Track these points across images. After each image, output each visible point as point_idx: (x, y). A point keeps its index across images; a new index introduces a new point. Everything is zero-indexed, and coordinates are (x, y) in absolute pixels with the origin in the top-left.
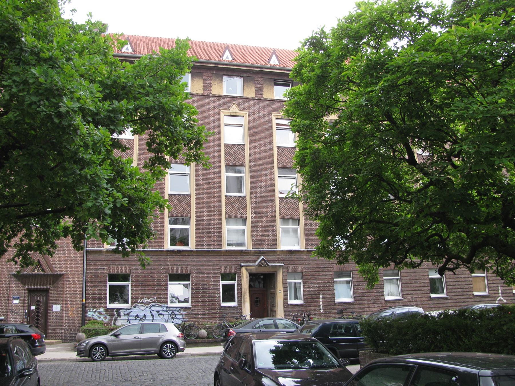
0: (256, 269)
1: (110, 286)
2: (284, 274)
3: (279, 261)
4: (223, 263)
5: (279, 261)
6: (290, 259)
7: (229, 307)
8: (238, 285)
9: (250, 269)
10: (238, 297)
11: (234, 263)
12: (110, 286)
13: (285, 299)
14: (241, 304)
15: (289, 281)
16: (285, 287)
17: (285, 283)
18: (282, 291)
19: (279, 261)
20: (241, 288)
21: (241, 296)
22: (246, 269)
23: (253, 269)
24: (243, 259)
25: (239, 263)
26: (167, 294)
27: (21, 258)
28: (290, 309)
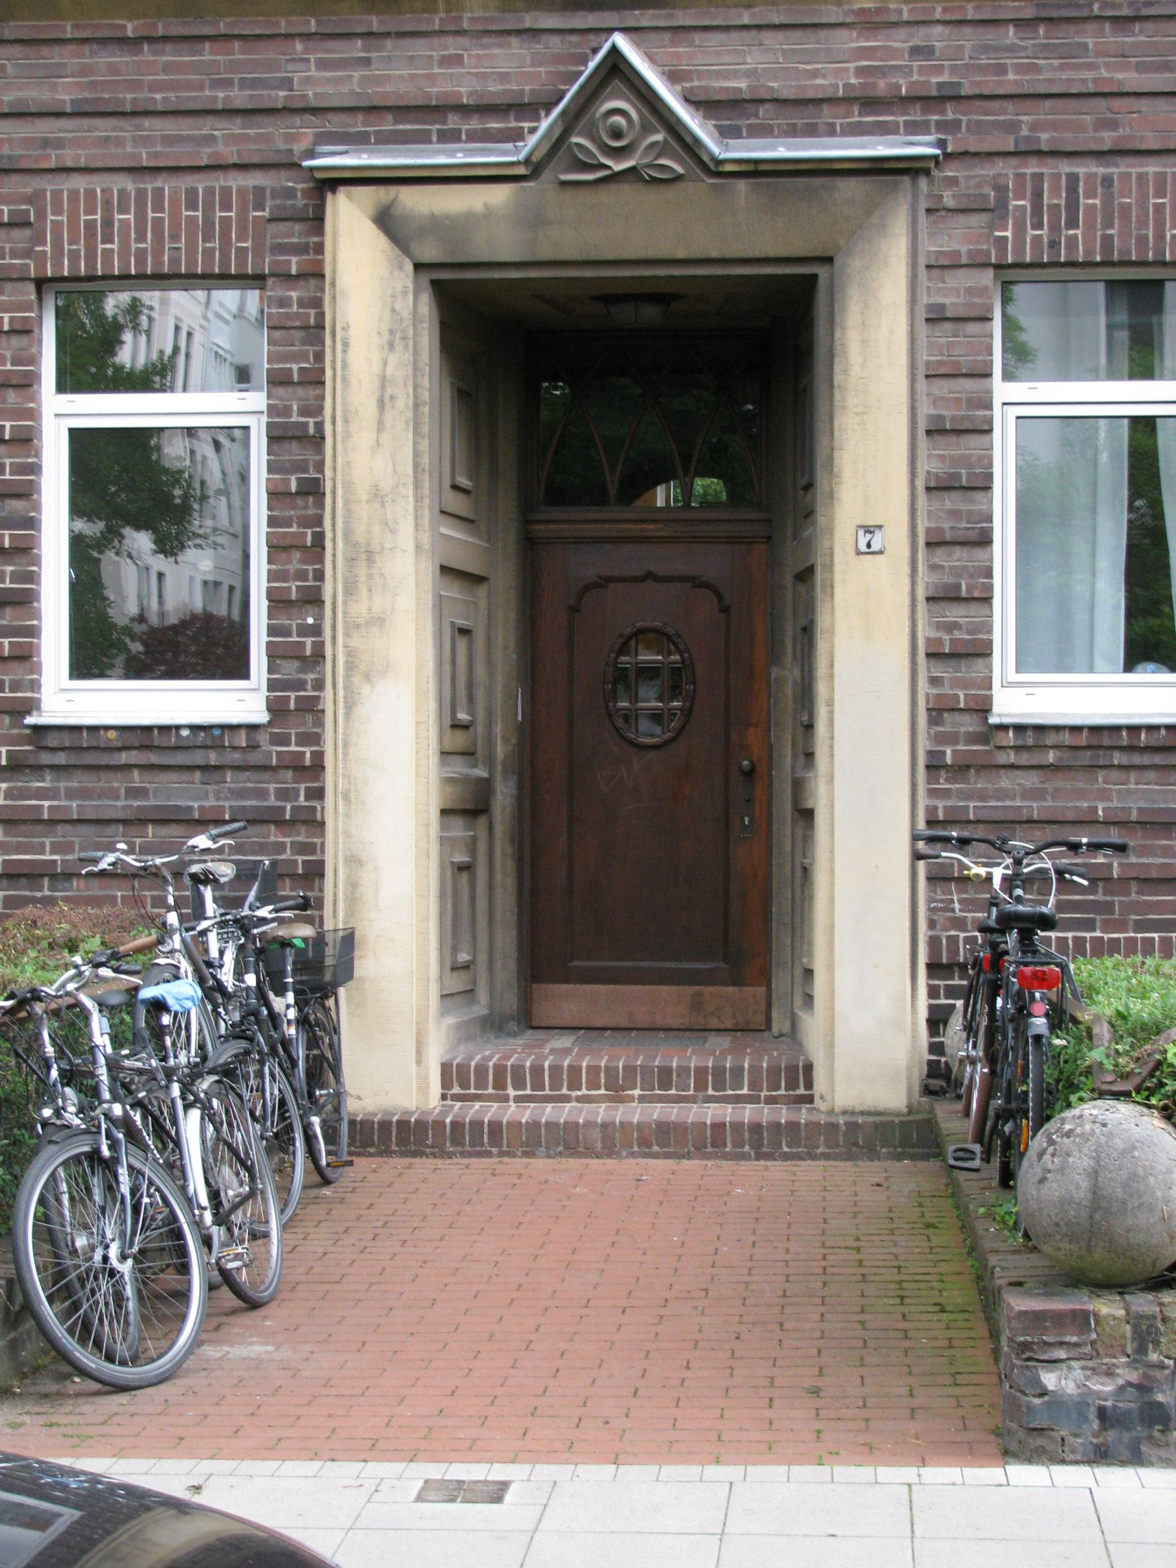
0: (532, 221)
1: (81, 440)
2: (953, 291)
3: (870, 105)
4: (81, 141)
5: (870, 103)
6: (1053, 74)
7: (143, 737)
8: (276, 437)
9: (438, 225)
10: (278, 602)
11: (225, 139)
12: (81, 440)
13: (953, 655)
14: (311, 707)
15: (1014, 398)
16: (953, 490)
17: (952, 431)
18: (896, 538)
19: (870, 103)
20: (313, 490)
21: (313, 599)
22: (385, 220)
23: (487, 218)
24: (349, 85)
25: (277, 136)
26: (272, 685)
27: (130, 1262)
28: (1013, 793)
